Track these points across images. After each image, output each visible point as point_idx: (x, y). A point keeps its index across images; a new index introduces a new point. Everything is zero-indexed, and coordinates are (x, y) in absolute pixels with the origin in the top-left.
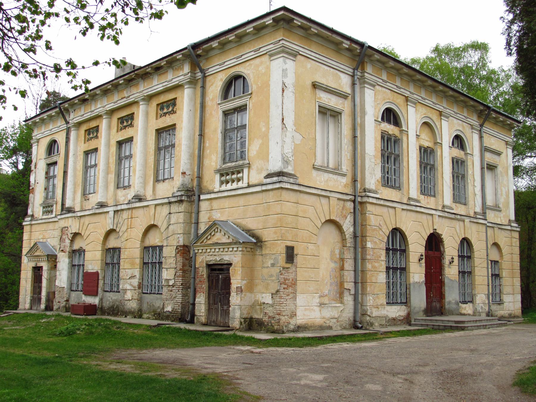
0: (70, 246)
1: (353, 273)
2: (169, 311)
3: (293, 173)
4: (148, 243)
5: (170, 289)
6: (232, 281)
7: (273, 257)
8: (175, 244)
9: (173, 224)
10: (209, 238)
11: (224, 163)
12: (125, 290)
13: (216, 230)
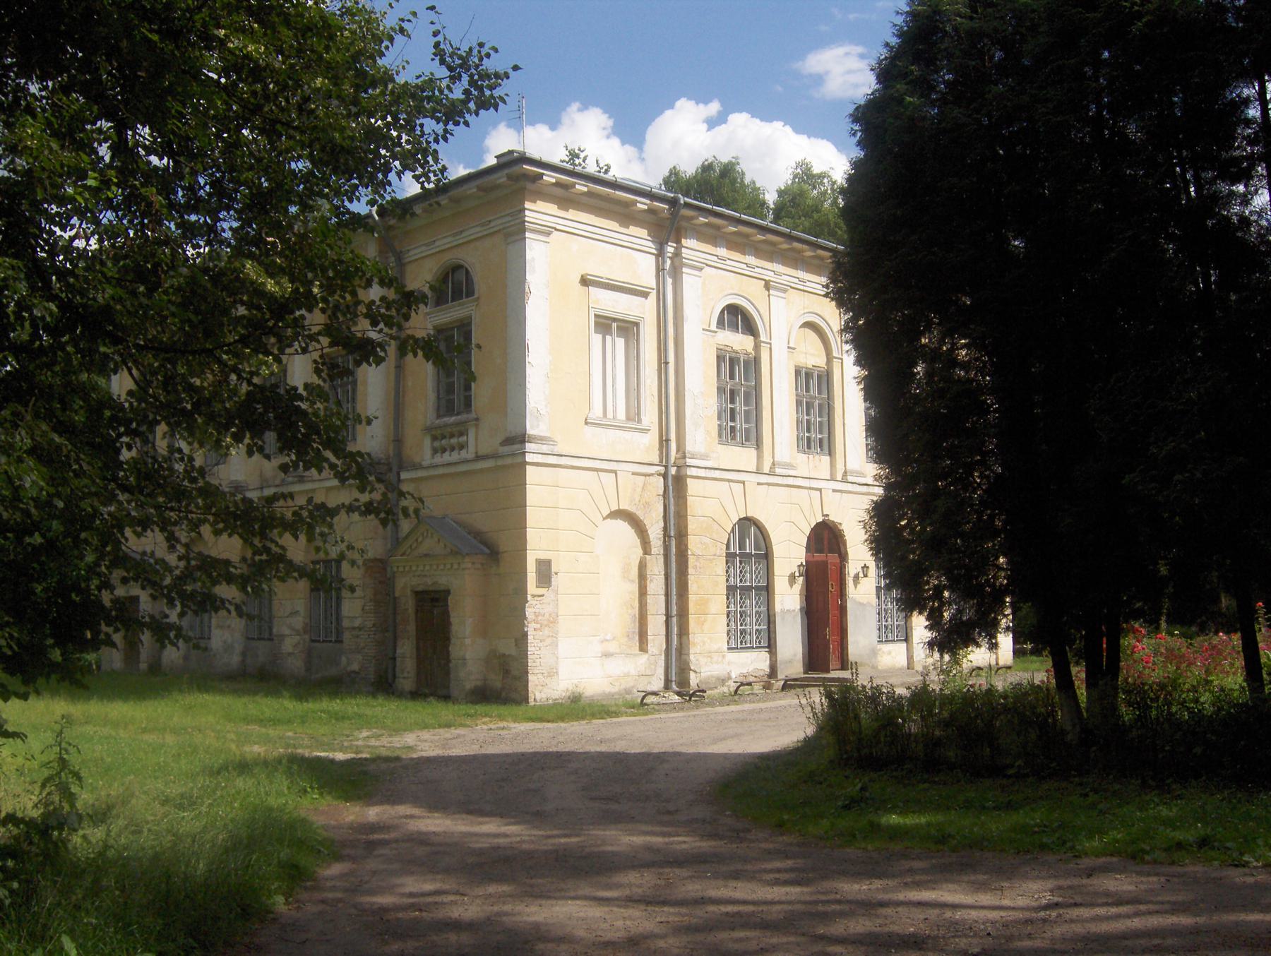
3: (547, 434)
11: (439, 417)
12: (282, 636)
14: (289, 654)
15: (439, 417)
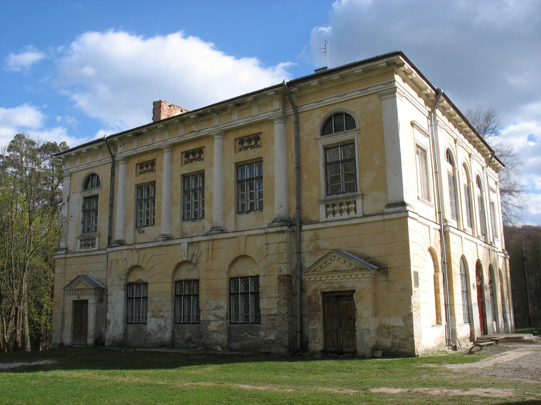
2: (271, 340)
6: (357, 307)
9: (272, 255)
12: (209, 322)
14: (214, 331)
15: (327, 195)
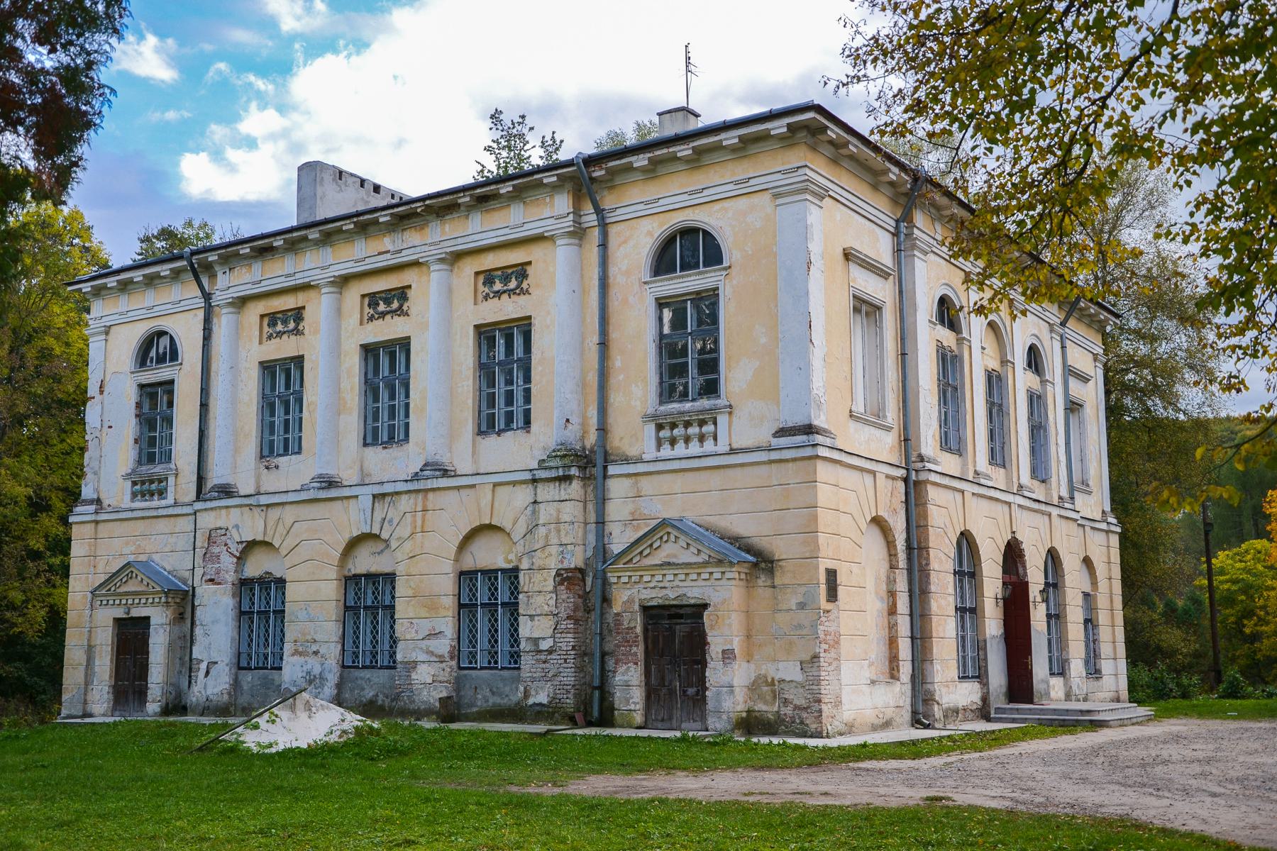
0: (236, 571)
1: (908, 618)
2: (541, 704)
4: (468, 563)
5: (543, 657)
6: (709, 639)
7: (803, 589)
8: (553, 564)
10: (645, 553)
11: (661, 403)
12: (413, 665)
13: (665, 538)
15: (661, 403)
